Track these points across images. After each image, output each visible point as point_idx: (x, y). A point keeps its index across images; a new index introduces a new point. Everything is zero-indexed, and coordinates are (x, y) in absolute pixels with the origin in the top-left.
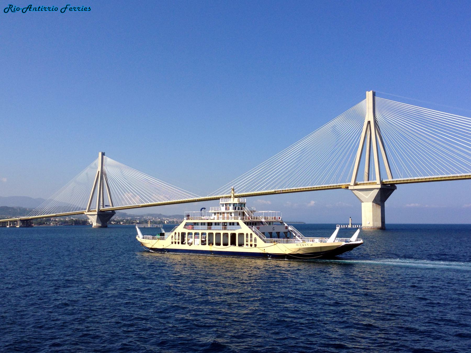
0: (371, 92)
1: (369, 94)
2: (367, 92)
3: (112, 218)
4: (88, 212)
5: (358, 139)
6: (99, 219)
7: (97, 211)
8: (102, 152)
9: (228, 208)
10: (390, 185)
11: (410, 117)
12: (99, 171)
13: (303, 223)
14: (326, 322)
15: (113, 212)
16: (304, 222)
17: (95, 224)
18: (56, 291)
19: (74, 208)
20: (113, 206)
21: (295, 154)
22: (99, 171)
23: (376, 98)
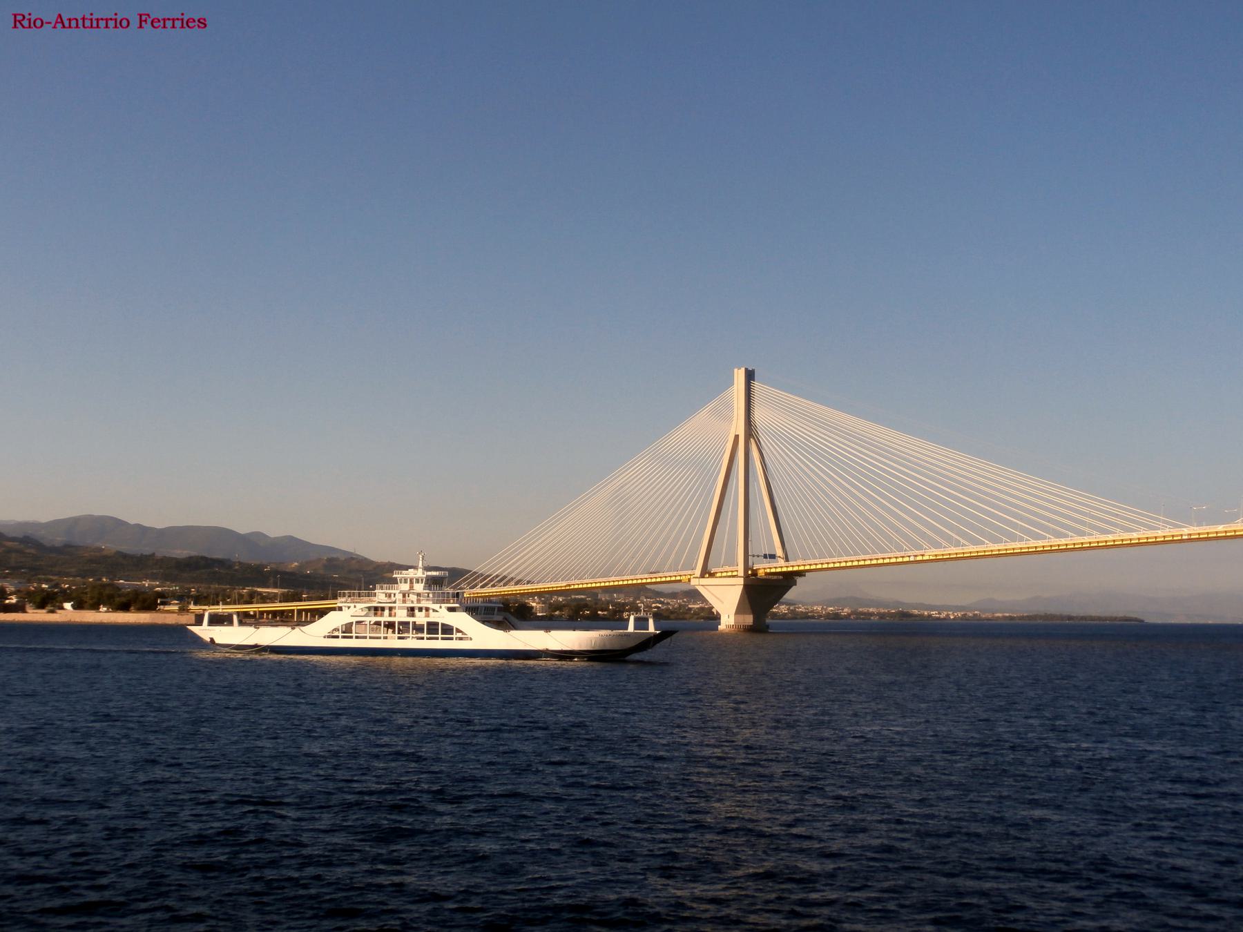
0: (743, 369)
1: (740, 376)
2: (736, 370)
3: (785, 596)
4: (702, 576)
5: (719, 461)
6: (747, 601)
7: (741, 573)
8: (746, 370)
9: (393, 614)
10: (781, 577)
11: (810, 417)
12: (737, 437)
13: (1136, 620)
14: (111, 741)
15: (789, 579)
16: (1141, 617)
17: (728, 620)
18: (258, 777)
19: (505, 577)
20: (787, 560)
21: (652, 489)
22: (737, 437)
23: (757, 386)
